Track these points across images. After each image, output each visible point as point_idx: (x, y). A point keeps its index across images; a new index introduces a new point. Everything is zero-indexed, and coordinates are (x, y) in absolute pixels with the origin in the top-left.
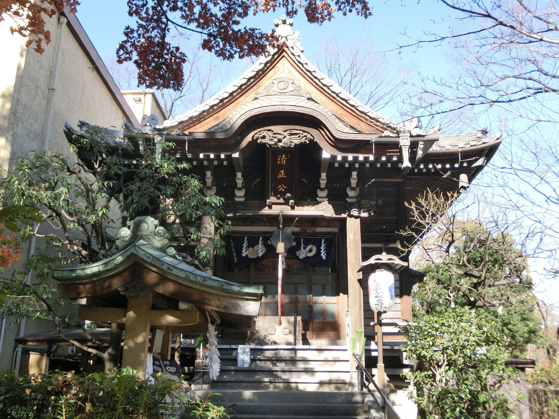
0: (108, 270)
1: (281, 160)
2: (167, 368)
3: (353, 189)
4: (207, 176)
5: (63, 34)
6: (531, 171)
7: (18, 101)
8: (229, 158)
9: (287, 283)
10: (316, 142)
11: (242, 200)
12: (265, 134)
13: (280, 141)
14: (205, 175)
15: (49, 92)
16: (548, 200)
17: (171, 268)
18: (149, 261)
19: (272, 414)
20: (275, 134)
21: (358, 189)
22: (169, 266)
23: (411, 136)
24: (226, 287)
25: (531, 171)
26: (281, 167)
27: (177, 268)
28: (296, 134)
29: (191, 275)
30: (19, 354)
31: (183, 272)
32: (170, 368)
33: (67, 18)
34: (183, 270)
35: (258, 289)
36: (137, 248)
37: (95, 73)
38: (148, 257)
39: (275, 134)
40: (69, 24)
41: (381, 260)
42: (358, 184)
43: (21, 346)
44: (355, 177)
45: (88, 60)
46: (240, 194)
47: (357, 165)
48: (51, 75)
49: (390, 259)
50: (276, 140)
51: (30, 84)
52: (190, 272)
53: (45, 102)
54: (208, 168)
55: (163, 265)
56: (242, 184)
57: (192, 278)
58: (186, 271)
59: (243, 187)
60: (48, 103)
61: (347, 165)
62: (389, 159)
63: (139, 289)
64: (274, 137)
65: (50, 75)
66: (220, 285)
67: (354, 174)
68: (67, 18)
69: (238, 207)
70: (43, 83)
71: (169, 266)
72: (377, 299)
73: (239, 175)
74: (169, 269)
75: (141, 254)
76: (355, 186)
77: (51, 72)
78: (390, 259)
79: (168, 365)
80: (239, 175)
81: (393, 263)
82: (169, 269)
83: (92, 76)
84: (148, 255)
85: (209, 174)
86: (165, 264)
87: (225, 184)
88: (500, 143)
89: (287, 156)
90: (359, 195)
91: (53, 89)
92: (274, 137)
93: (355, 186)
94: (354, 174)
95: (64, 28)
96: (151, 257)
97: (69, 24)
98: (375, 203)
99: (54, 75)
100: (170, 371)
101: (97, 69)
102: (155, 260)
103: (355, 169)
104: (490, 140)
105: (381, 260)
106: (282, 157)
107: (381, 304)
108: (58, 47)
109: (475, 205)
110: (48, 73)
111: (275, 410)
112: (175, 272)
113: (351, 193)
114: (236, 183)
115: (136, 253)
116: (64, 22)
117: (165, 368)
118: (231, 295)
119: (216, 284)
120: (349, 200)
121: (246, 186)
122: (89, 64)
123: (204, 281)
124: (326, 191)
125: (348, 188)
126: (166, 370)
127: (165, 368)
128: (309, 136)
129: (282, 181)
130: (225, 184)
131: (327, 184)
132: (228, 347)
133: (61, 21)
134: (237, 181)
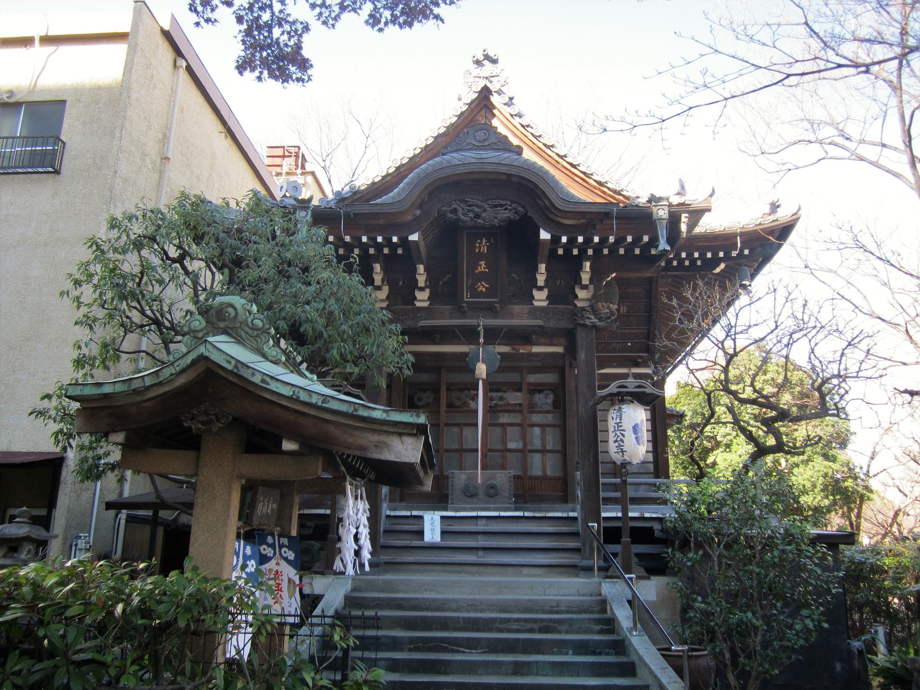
0: (160, 384)
1: (480, 247)
2: (283, 550)
3: (585, 287)
4: (375, 271)
5: (180, 84)
6: (831, 271)
7: (116, 172)
8: (404, 242)
9: (491, 425)
10: (530, 218)
11: (426, 304)
12: (455, 206)
13: (477, 216)
14: (372, 269)
15: (162, 162)
16: (856, 310)
17: (268, 379)
18: (229, 367)
19: (468, 611)
20: (470, 206)
21: (592, 287)
22: (265, 377)
23: (670, 205)
24: (362, 412)
25: (831, 271)
26: (481, 256)
27: (277, 380)
28: (502, 206)
29: (301, 391)
30: (123, 522)
31: (289, 387)
32: (286, 550)
33: (186, 60)
34: (288, 384)
35: (418, 416)
36: (208, 346)
37: (229, 141)
38: (229, 362)
39: (470, 206)
40: (189, 69)
41: (626, 387)
42: (591, 280)
43: (124, 511)
44: (588, 269)
45: (219, 122)
46: (422, 298)
47: (590, 252)
48: (165, 140)
49: (639, 387)
50: (471, 215)
51: (133, 149)
52: (301, 388)
53: (156, 176)
54: (375, 258)
55: (253, 374)
56: (426, 282)
57: (303, 397)
58: (293, 385)
59: (426, 287)
60: (160, 178)
61: (575, 252)
62: (637, 240)
63: (213, 417)
64: (469, 211)
65: (164, 139)
66: (352, 409)
67: (587, 265)
68: (186, 60)
69: (419, 315)
70: (153, 149)
71: (265, 377)
72: (617, 444)
73: (421, 268)
74: (263, 381)
75: (216, 357)
76: (587, 283)
77: (165, 134)
78: (639, 387)
79: (286, 546)
80: (421, 268)
81: (644, 392)
82: (263, 381)
83: (223, 144)
84: (229, 359)
85: (377, 267)
86: (257, 373)
87: (401, 283)
88: (798, 219)
89: (489, 241)
90: (594, 296)
91: (167, 158)
92: (469, 211)
93: (587, 283)
94: (587, 265)
95: (183, 75)
96: (233, 362)
97: (189, 69)
98: (616, 307)
99: (168, 139)
100: (285, 555)
101: (224, 123)
102: (240, 366)
103: (588, 258)
104: (783, 215)
105: (626, 387)
106: (480, 243)
107: (622, 452)
108: (174, 101)
109: (758, 311)
110: (160, 136)
111: (472, 605)
112: (273, 386)
113: (581, 294)
114: (417, 281)
115: (206, 354)
116: (182, 67)
117: (280, 551)
118: (384, 428)
119: (344, 408)
120: (579, 304)
121: (432, 283)
122: (220, 128)
123: (323, 402)
124: (546, 290)
125: (576, 286)
126: (281, 554)
127: (280, 551)
128: (520, 208)
129: (482, 277)
130: (401, 283)
131: (546, 280)
132: (408, 513)
133: (178, 64)
134: (418, 277)
